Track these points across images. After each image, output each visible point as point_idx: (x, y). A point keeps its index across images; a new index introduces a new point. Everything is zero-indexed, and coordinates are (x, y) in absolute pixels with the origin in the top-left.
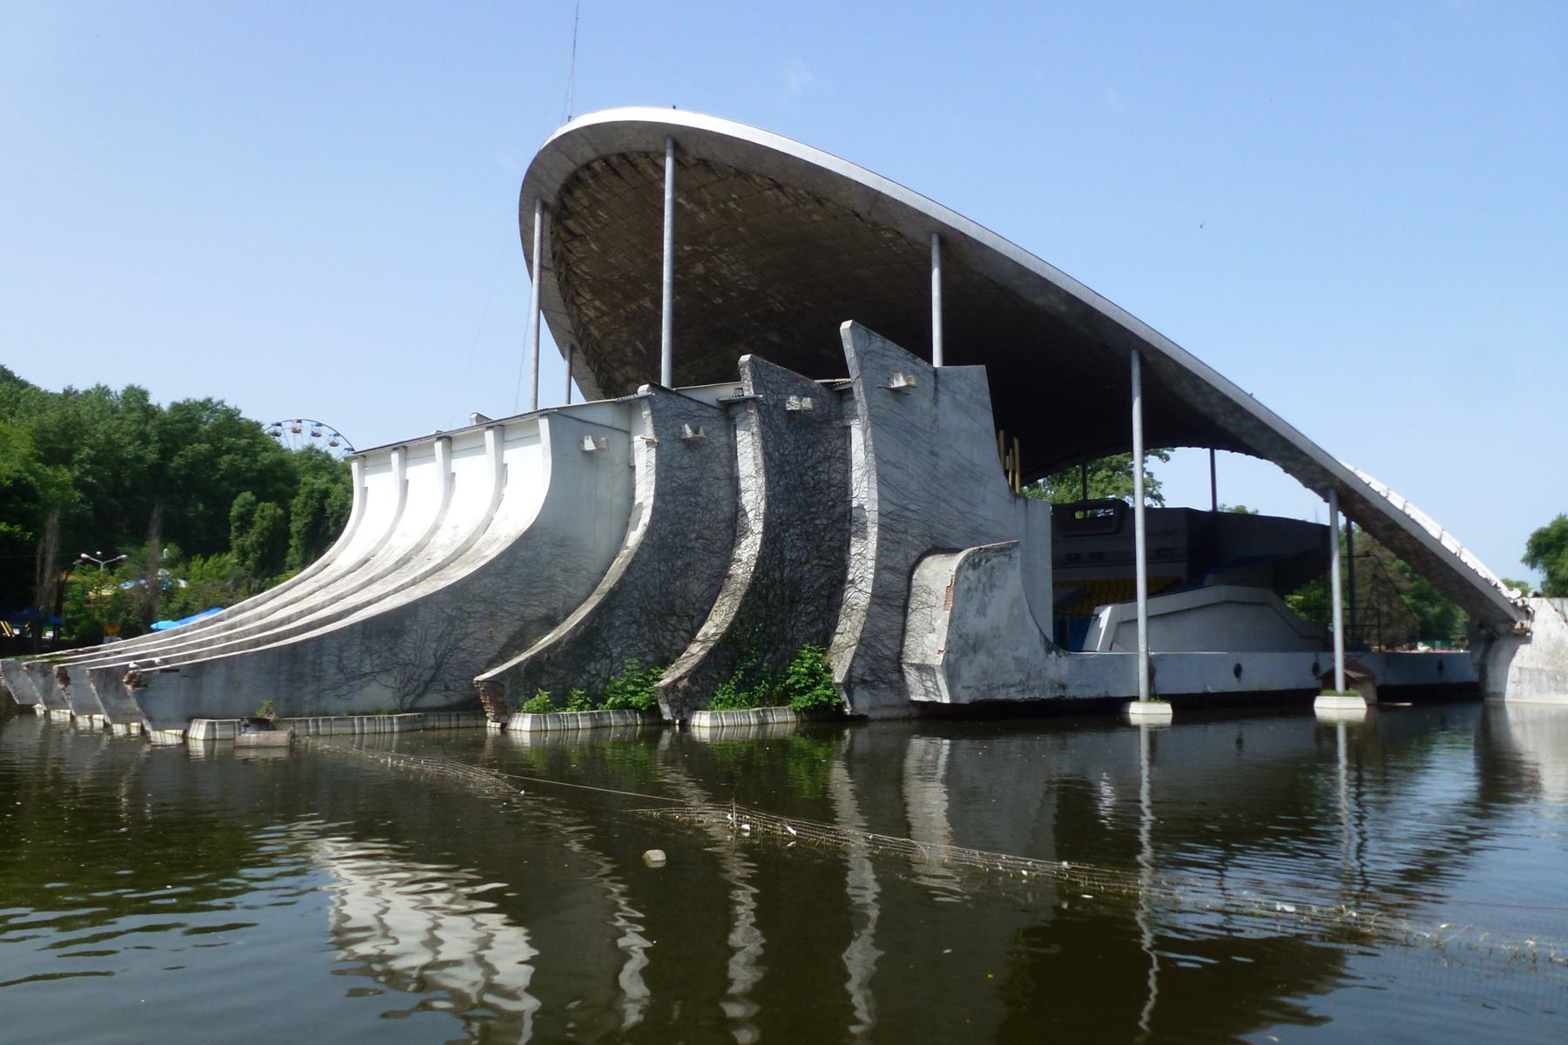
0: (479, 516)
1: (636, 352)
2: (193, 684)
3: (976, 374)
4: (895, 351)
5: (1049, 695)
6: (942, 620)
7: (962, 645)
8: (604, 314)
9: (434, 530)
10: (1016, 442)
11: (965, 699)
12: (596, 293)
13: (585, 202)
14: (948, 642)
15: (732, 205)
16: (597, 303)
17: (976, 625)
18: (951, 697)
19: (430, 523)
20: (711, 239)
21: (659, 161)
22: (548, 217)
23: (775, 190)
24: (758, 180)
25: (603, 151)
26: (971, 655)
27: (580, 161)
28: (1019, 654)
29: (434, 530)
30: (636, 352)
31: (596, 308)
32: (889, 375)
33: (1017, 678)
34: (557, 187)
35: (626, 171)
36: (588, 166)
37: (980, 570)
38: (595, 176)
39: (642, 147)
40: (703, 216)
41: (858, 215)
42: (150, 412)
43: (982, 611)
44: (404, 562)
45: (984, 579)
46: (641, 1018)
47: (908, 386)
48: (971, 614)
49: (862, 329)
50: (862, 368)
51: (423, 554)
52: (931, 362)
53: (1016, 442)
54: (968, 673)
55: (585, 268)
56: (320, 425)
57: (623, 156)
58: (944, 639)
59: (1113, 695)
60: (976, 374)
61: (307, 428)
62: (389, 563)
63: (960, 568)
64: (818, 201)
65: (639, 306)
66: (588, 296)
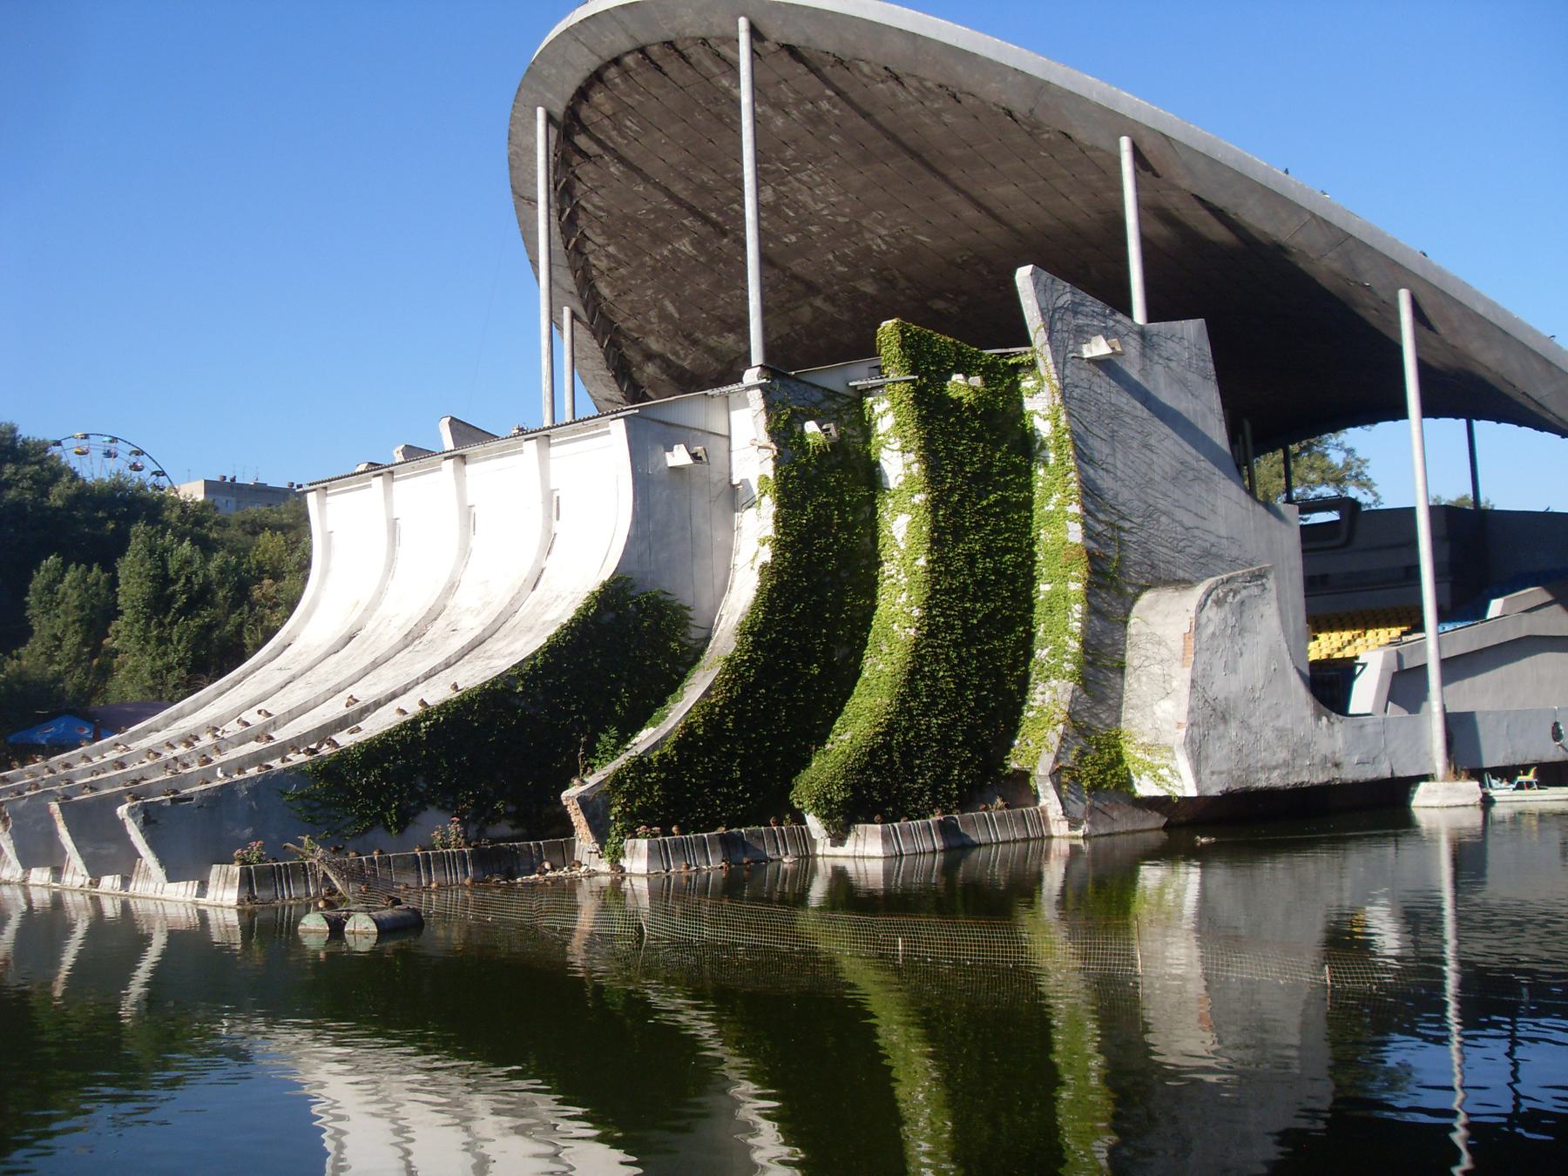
0: (523, 569)
1: (664, 316)
2: (189, 827)
3: (1192, 329)
4: (1094, 305)
5: (1320, 778)
6: (1181, 678)
7: (1210, 715)
8: (619, 263)
9: (452, 588)
10: (1247, 425)
11: (1214, 791)
12: (611, 235)
13: (607, 108)
14: (1191, 711)
15: (825, 105)
16: (611, 249)
17: (1224, 686)
18: (1199, 782)
19: (443, 581)
20: (789, 153)
21: (725, 50)
22: (554, 132)
23: (892, 84)
24: (866, 69)
25: (643, 38)
26: (1221, 728)
27: (607, 55)
28: (1280, 723)
29: (452, 588)
30: (664, 316)
31: (609, 256)
32: (1082, 335)
33: (1282, 755)
34: (570, 90)
35: (672, 66)
36: (616, 61)
37: (1227, 607)
38: (625, 73)
39: (700, 32)
40: (779, 121)
41: (1010, 113)
42: (14, 440)
43: (1230, 668)
44: (411, 638)
45: (1232, 621)
46: (1265, 1170)
47: (1115, 353)
48: (1218, 673)
49: (1045, 276)
50: (1050, 331)
51: (441, 622)
52: (1127, 311)
53: (1247, 425)
54: (1220, 754)
55: (596, 200)
56: (114, 440)
57: (670, 44)
58: (1185, 708)
59: (1398, 774)
60: (1192, 329)
61: (98, 445)
62: (393, 635)
63: (1201, 607)
64: (897, 78)
65: (674, 252)
66: (600, 240)
